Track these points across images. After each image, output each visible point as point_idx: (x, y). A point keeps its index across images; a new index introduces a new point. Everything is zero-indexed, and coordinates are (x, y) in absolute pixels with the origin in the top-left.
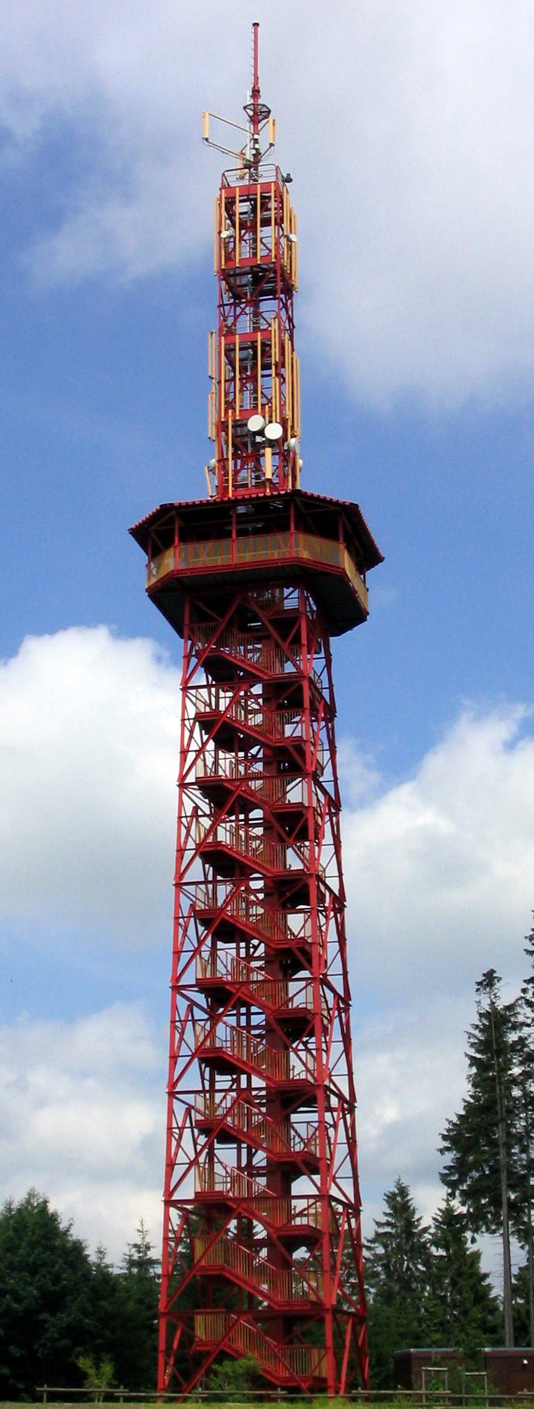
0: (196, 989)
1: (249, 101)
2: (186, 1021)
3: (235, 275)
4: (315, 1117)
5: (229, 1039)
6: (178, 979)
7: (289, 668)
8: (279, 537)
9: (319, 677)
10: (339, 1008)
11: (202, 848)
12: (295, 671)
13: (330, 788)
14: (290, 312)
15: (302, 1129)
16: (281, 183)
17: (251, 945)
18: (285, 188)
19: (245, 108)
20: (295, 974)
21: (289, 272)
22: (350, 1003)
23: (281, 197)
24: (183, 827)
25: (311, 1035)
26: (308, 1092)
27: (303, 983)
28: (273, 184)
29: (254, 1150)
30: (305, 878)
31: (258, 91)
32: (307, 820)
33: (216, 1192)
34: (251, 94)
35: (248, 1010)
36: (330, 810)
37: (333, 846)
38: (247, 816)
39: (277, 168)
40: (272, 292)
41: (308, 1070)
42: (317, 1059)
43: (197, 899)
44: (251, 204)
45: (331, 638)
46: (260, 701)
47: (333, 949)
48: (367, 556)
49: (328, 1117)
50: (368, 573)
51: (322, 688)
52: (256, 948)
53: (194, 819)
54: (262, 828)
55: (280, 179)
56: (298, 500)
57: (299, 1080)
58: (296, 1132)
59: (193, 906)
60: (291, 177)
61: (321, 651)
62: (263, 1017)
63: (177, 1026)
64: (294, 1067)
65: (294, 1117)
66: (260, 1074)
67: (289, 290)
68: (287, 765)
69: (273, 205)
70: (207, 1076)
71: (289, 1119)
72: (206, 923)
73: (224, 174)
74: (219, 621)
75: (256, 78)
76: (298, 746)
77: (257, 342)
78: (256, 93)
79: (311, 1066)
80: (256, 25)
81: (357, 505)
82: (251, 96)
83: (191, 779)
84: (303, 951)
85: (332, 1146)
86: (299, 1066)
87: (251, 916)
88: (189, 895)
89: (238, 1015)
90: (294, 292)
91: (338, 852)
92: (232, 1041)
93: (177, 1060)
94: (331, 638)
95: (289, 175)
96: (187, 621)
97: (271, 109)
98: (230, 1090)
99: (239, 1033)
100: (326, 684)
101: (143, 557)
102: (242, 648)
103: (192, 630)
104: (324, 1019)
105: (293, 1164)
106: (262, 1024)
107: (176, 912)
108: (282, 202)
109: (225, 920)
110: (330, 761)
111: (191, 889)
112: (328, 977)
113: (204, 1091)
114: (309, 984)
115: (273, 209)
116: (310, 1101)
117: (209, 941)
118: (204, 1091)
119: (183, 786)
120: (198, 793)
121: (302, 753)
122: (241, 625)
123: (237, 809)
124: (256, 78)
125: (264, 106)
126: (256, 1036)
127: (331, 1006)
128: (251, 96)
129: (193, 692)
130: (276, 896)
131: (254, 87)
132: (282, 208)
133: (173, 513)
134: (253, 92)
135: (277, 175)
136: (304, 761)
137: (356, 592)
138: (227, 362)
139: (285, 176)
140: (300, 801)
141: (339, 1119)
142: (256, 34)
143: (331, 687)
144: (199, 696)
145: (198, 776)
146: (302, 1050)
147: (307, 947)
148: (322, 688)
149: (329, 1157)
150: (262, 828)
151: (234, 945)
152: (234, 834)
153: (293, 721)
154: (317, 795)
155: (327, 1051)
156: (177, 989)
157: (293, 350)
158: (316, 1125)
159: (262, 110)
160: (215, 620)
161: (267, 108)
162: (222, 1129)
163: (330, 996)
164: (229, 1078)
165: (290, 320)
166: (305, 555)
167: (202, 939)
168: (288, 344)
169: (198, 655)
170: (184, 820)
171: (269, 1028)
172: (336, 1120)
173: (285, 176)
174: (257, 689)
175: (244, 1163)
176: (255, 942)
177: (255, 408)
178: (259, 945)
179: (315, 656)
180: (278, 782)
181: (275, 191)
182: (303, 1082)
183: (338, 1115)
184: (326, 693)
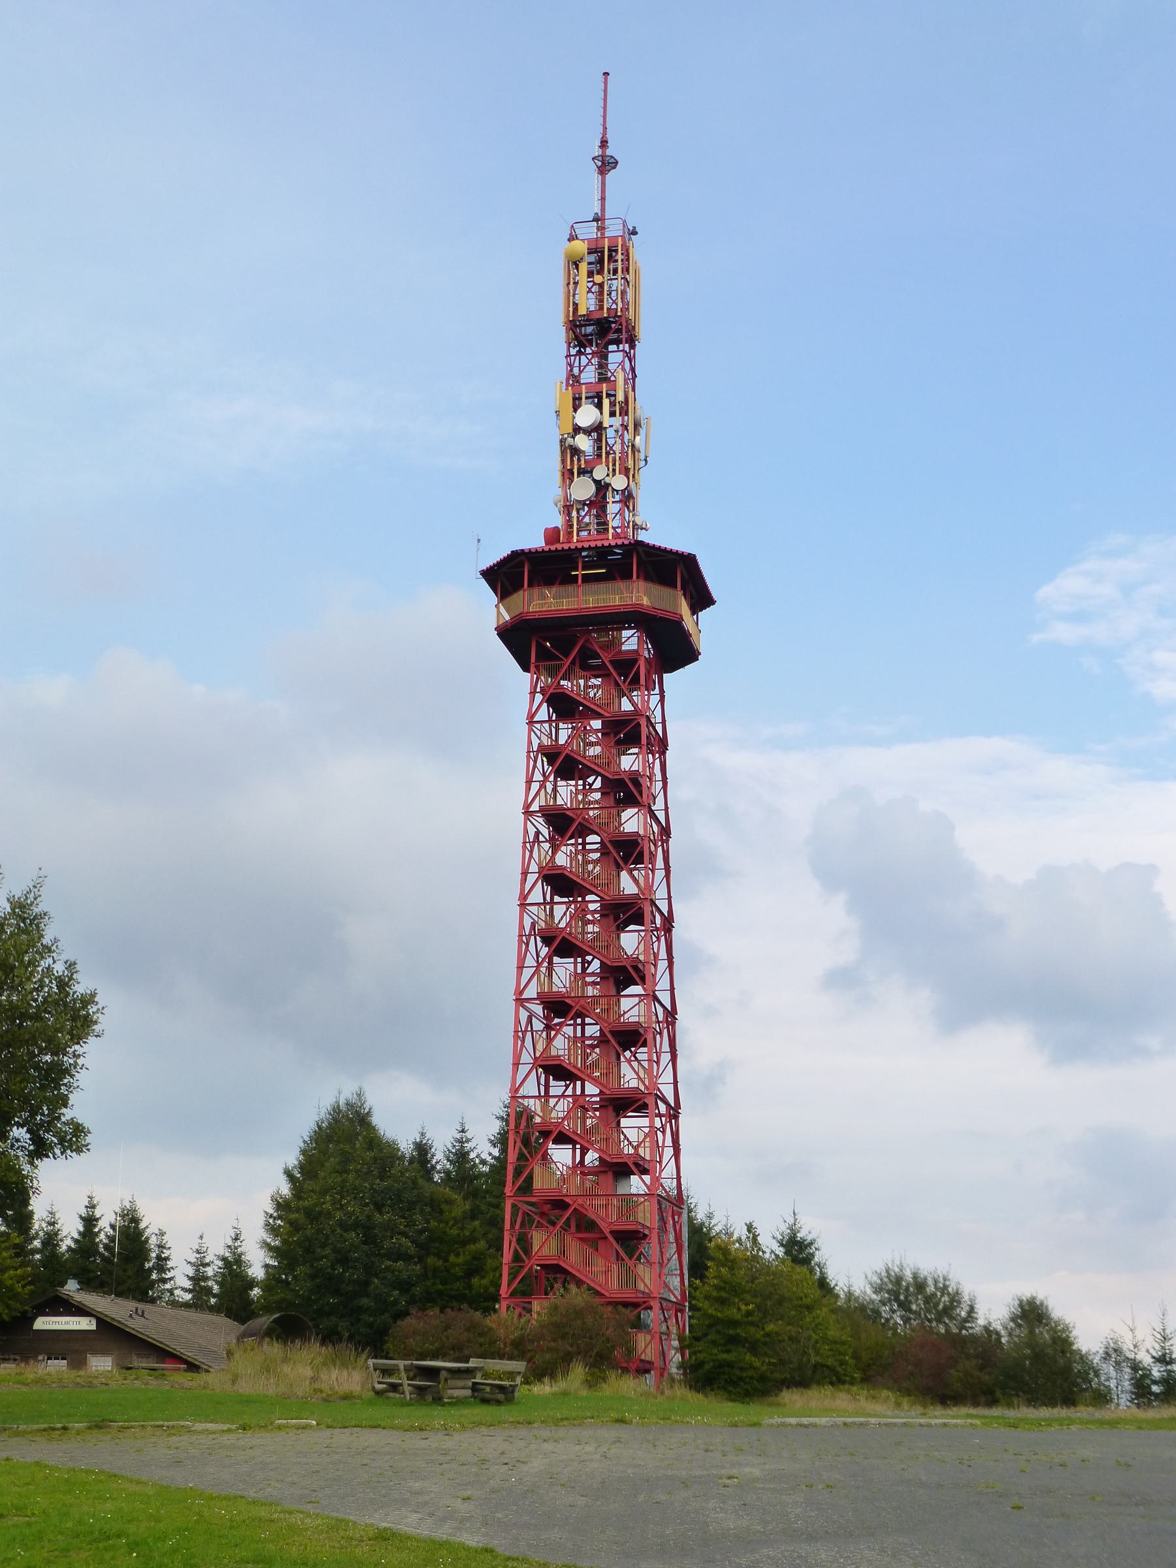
0: (538, 1002)
1: (597, 152)
2: (530, 935)
3: (581, 326)
4: (645, 1122)
5: (566, 1048)
6: (521, 993)
7: (626, 705)
8: (621, 585)
9: (653, 712)
10: (667, 1022)
11: (552, 689)
12: (633, 709)
13: (661, 816)
14: (633, 364)
15: (633, 1135)
16: (627, 236)
17: (587, 783)
18: (631, 242)
19: (593, 159)
20: (627, 927)
21: (633, 325)
22: (680, 1111)
23: (627, 251)
24: (531, 760)
25: (644, 1044)
26: (640, 1099)
27: (636, 1000)
28: (620, 238)
29: (586, 965)
30: (639, 902)
31: (607, 142)
32: (642, 847)
33: (553, 1057)
34: (600, 144)
35: (583, 1021)
36: (662, 838)
37: (667, 900)
38: (584, 840)
39: (624, 222)
40: (617, 342)
41: (639, 1078)
42: (649, 1071)
43: (539, 918)
44: (598, 255)
45: (664, 675)
46: (600, 735)
47: (663, 965)
48: (701, 599)
49: (658, 1123)
50: (700, 613)
51: (656, 723)
52: (590, 963)
53: (536, 844)
54: (600, 793)
55: (626, 230)
56: (640, 549)
57: (628, 1022)
58: (625, 1136)
59: (533, 925)
60: (637, 230)
61: (655, 688)
62: (598, 1027)
63: (519, 1035)
64: (625, 1075)
65: (624, 1122)
66: (595, 1081)
67: (632, 341)
68: (622, 794)
69: (619, 257)
70: (542, 1081)
71: (619, 1123)
72: (547, 941)
73: (572, 227)
74: (563, 660)
75: (605, 128)
76: (635, 778)
77: (602, 392)
78: (604, 144)
79: (642, 1074)
80: (606, 74)
81: (694, 555)
82: (600, 147)
83: (535, 807)
84: (636, 968)
85: (660, 1149)
86: (629, 1077)
87: (589, 933)
88: (530, 913)
89: (575, 1025)
90: (637, 342)
91: (674, 1059)
92: (569, 1049)
93: (522, 970)
94: (664, 675)
95: (634, 227)
96: (533, 659)
97: (618, 160)
98: (563, 1096)
99: (575, 1043)
100: (659, 719)
101: (494, 599)
102: (582, 682)
103: (537, 667)
104: (653, 936)
105: (623, 969)
106: (595, 1035)
107: (524, 838)
108: (628, 255)
109: (566, 938)
110: (662, 790)
111: (534, 909)
112: (656, 992)
113: (539, 1097)
114: (642, 1000)
115: (620, 261)
116: (638, 919)
117: (552, 778)
118: (539, 1097)
119: (528, 813)
120: (541, 820)
121: (638, 785)
122: (586, 664)
123: (577, 835)
124: (605, 128)
125: (612, 157)
126: (589, 1046)
127: (661, 1019)
128: (600, 147)
129: (538, 726)
130: (612, 917)
131: (603, 138)
132: (628, 260)
133: (523, 557)
134: (601, 142)
135: (624, 230)
136: (641, 793)
137: (690, 635)
138: (573, 337)
139: (631, 228)
140: (636, 830)
141: (666, 1122)
142: (606, 83)
143: (664, 722)
144: (543, 730)
145: (541, 805)
146: (633, 1061)
147: (640, 966)
148: (656, 723)
149: (658, 1160)
150: (600, 793)
151: (572, 960)
152: (572, 857)
153: (628, 752)
154: (651, 826)
155: (658, 1063)
156: (520, 1001)
157: (635, 400)
158: (647, 1130)
159: (610, 161)
160: (562, 660)
161: (615, 159)
162: (560, 1131)
163: (660, 1011)
164: (563, 1083)
165: (633, 369)
166: (645, 601)
167: (547, 774)
168: (631, 394)
169: (543, 692)
170: (528, 845)
171: (603, 851)
172: (664, 1123)
173: (631, 228)
174: (597, 724)
175: (578, 1159)
176: (589, 958)
177: (599, 456)
178: (593, 960)
179: (652, 693)
180: (614, 811)
181: (622, 245)
182: (637, 1024)
183: (666, 1119)
184: (659, 728)
